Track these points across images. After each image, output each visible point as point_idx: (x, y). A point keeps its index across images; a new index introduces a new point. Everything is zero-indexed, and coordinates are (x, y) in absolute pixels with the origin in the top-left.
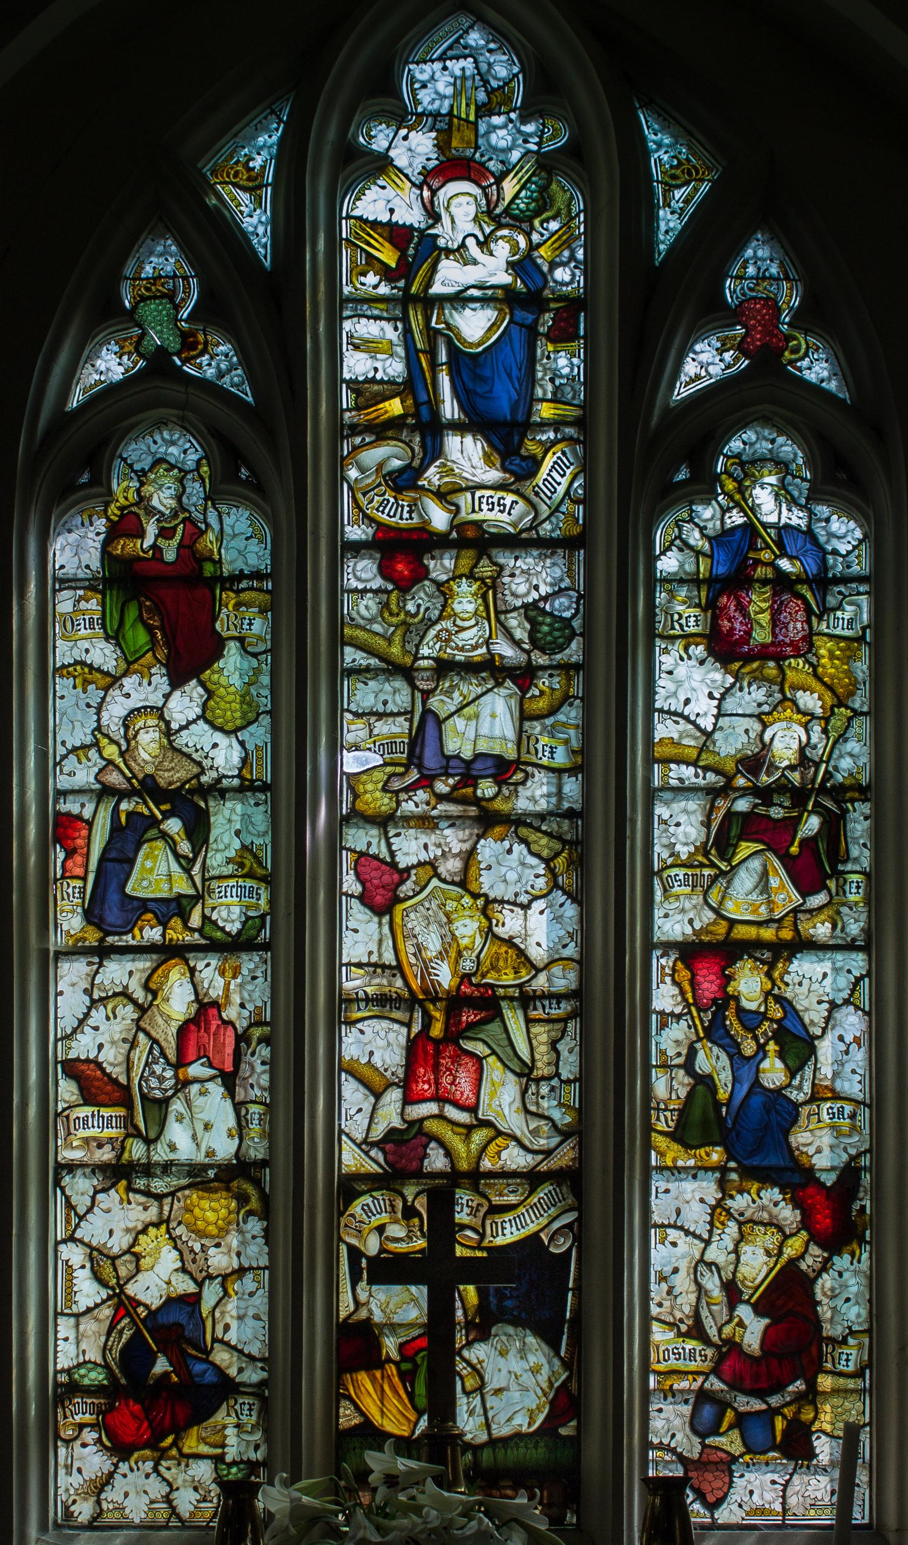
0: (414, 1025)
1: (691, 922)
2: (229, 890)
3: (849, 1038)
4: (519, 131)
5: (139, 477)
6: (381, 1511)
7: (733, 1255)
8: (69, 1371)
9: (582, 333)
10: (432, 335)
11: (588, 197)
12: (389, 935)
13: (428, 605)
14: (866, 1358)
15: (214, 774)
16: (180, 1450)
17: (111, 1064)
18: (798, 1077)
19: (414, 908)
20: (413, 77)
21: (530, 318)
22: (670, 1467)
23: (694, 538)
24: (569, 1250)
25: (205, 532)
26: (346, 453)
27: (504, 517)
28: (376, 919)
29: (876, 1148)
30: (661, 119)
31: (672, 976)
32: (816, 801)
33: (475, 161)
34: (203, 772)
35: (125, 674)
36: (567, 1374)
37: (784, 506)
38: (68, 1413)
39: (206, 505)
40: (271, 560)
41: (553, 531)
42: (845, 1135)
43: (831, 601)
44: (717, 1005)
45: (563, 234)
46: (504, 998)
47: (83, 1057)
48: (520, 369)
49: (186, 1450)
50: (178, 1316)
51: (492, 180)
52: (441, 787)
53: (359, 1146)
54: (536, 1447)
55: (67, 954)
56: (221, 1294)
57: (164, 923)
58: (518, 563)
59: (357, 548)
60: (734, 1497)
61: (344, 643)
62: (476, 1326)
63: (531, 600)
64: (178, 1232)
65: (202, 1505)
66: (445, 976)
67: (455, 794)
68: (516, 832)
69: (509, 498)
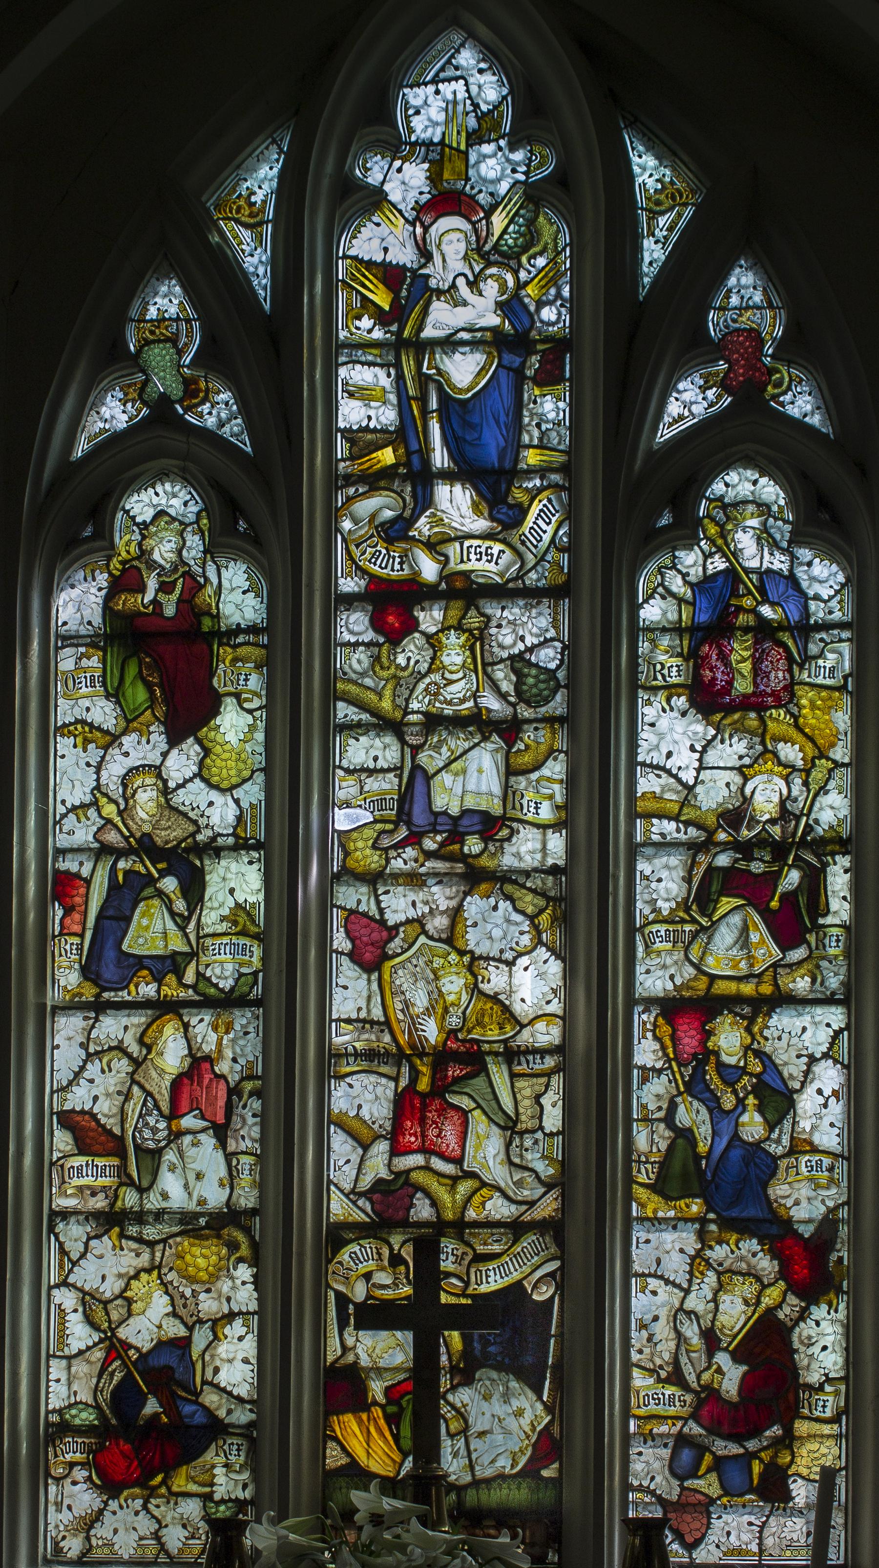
0: (401, 1079)
1: (672, 977)
2: (222, 947)
3: (827, 1092)
4: (508, 160)
5: (141, 530)
6: (367, 1549)
7: (712, 1304)
8: (60, 1412)
9: (568, 375)
10: (423, 380)
11: (574, 230)
12: (378, 992)
13: (418, 657)
14: (842, 1404)
15: (210, 833)
16: (169, 1489)
17: (105, 1116)
18: (777, 1131)
19: (402, 965)
20: (407, 103)
21: (517, 361)
22: (650, 1508)
23: (676, 584)
24: (552, 1297)
25: (204, 586)
26: (340, 504)
27: (492, 567)
28: (365, 976)
29: (854, 1201)
30: (645, 139)
31: (654, 1031)
32: (796, 855)
33: (466, 194)
34: (198, 831)
35: (125, 732)
36: (549, 1418)
37: (766, 550)
38: (59, 1452)
39: (205, 558)
40: (268, 614)
41: (538, 580)
42: (823, 1188)
43: (813, 649)
44: (697, 1060)
45: (550, 271)
46: (490, 1053)
47: (78, 1109)
48: (507, 415)
49: (175, 1489)
50: (168, 1359)
51: (482, 215)
52: (430, 844)
53: (347, 1196)
54: (519, 1488)
55: (63, 1008)
56: (211, 1338)
57: (159, 980)
58: (505, 614)
59: (349, 601)
60: (712, 1538)
61: (337, 699)
62: (460, 1371)
63: (517, 651)
64: (170, 1277)
65: (191, 1542)
66: (431, 1032)
67: (443, 851)
68: (501, 889)
69: (497, 547)
